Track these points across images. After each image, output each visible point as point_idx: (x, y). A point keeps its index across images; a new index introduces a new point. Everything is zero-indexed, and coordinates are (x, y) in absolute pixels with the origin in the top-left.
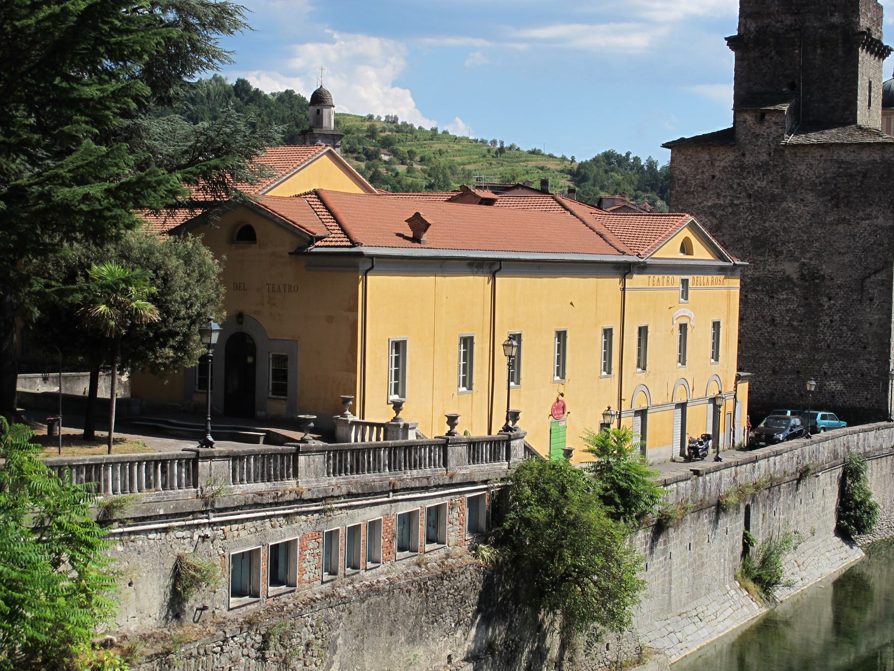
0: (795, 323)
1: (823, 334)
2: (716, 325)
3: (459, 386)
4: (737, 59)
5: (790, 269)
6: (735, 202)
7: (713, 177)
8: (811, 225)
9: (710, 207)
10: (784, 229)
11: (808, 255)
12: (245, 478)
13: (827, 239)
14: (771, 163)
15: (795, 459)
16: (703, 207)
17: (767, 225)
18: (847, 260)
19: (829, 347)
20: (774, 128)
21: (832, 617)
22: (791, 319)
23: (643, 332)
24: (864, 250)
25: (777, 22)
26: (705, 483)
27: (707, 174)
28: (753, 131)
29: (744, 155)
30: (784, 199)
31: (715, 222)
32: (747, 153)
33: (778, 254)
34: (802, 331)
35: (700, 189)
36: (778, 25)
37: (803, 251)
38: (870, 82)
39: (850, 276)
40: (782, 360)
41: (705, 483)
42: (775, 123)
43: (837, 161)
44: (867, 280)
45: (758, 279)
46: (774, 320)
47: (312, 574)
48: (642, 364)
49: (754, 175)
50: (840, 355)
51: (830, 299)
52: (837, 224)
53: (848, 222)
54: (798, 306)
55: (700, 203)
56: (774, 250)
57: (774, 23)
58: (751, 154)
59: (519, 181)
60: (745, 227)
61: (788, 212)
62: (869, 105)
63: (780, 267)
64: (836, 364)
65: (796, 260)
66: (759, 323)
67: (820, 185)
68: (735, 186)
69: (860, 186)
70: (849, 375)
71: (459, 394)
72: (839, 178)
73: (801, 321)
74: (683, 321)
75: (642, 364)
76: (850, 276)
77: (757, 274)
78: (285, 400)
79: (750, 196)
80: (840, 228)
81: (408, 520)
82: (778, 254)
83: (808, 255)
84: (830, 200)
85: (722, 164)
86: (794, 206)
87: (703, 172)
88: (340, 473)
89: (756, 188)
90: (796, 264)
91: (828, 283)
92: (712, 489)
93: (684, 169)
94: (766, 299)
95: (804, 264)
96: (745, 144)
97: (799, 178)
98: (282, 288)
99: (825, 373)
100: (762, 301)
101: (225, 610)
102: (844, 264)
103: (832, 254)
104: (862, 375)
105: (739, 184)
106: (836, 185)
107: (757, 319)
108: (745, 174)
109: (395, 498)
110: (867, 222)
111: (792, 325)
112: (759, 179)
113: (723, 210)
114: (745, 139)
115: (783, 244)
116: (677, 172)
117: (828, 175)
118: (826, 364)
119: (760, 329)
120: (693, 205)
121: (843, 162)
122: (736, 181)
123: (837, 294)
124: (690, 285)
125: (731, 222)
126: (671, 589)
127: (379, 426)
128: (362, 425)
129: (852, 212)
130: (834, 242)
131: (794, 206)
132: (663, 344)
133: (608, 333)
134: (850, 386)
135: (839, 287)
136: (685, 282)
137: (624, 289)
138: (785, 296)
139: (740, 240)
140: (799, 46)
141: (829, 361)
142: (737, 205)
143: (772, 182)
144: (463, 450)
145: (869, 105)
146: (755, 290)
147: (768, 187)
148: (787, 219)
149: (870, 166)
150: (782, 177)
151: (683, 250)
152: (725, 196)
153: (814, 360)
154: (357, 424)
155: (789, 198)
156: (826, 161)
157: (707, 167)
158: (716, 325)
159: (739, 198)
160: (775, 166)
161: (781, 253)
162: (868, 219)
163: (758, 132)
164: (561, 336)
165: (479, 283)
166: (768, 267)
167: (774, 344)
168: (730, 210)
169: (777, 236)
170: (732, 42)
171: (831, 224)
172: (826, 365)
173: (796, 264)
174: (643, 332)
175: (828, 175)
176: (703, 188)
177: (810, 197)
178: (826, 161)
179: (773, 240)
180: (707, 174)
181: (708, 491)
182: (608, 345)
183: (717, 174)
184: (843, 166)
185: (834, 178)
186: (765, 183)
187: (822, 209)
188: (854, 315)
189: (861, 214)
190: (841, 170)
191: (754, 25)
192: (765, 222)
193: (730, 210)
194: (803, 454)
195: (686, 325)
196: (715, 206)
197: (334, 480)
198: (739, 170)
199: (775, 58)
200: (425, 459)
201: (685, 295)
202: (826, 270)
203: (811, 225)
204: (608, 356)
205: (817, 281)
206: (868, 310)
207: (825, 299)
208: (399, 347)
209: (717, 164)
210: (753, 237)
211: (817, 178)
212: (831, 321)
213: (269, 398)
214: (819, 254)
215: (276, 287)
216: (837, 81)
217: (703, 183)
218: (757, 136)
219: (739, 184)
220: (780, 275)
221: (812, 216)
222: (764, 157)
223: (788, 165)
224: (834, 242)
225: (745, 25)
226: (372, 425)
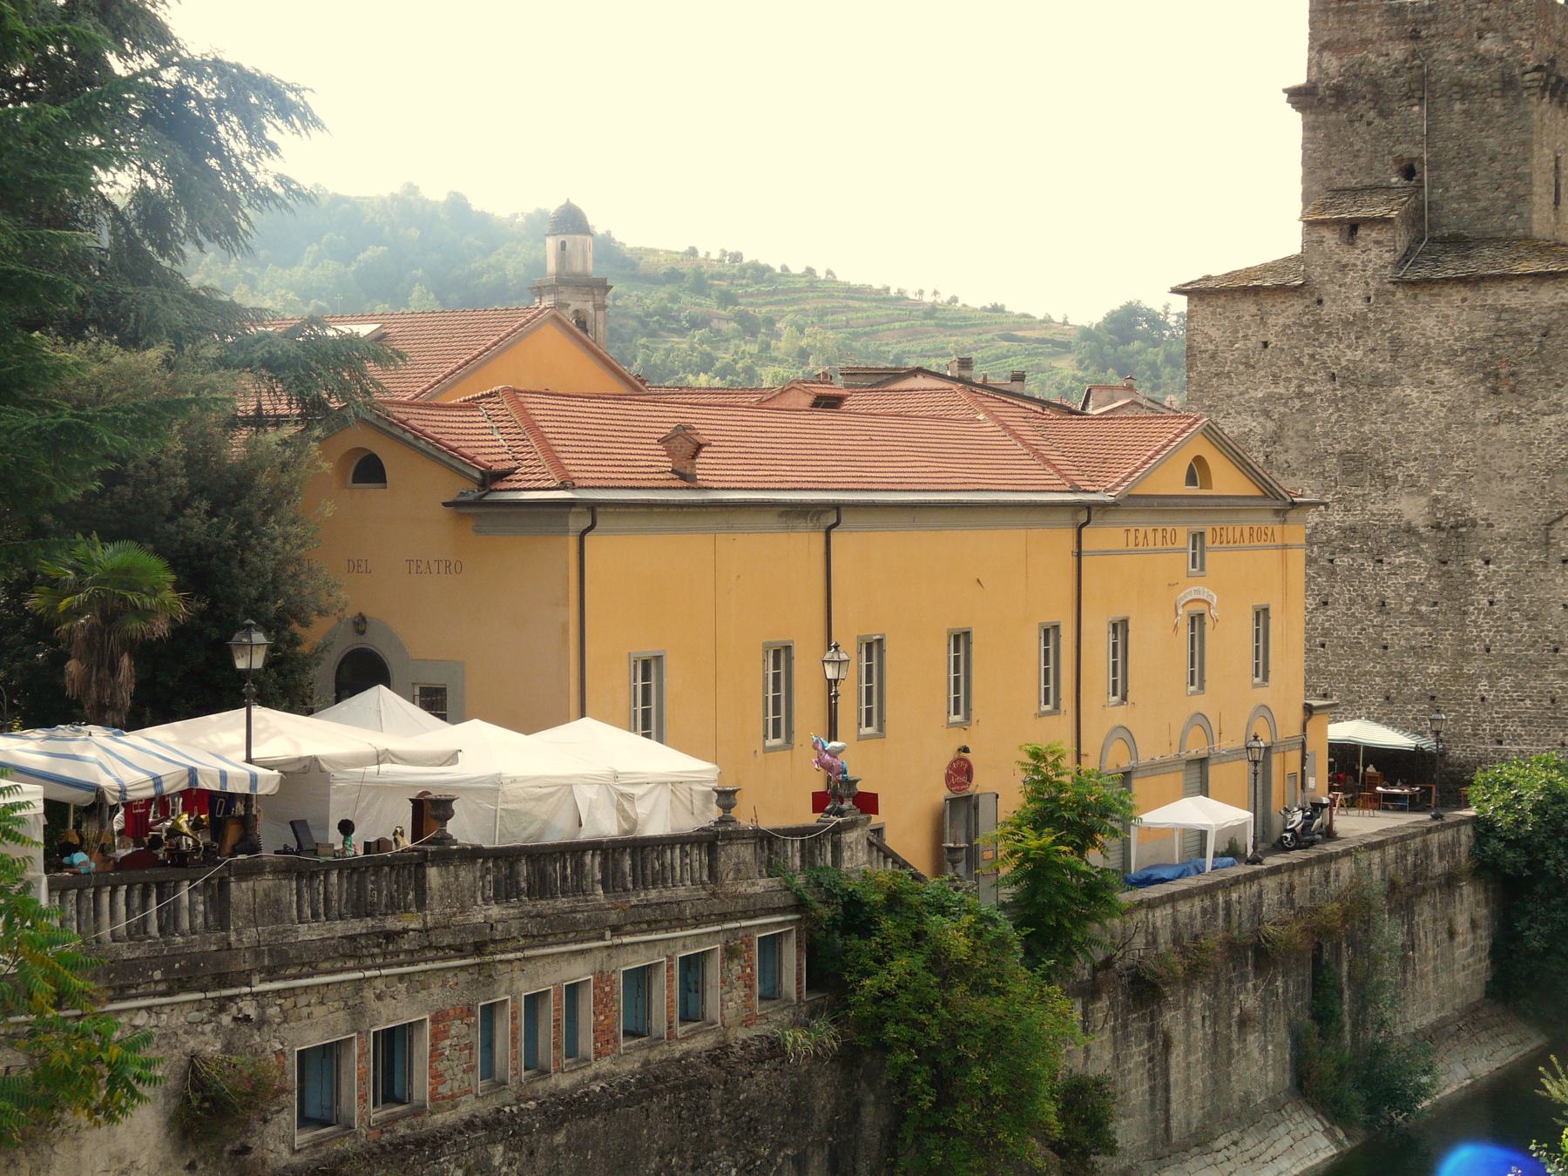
0: (1423, 608)
1: (1476, 627)
2: (1262, 614)
3: (766, 737)
4: (1306, 127)
5: (1412, 509)
6: (1307, 389)
7: (1266, 345)
8: (1448, 427)
9: (1261, 401)
10: (1399, 438)
11: (1445, 483)
12: (321, 910)
13: (1479, 452)
14: (1370, 315)
15: (1410, 859)
16: (1248, 401)
17: (1366, 428)
18: (1516, 490)
19: (1488, 650)
20: (1375, 251)
21: (653, 982)
22: (1416, 602)
23: (1120, 628)
24: (1550, 471)
25: (1380, 55)
26: (1228, 904)
27: (1254, 339)
28: (1336, 258)
29: (1320, 302)
30: (1396, 381)
31: (1271, 426)
32: (1325, 298)
33: (1387, 482)
34: (1436, 622)
35: (1241, 367)
37: (1435, 476)
38: (1557, 159)
39: (1525, 519)
40: (1402, 676)
41: (1228, 904)
42: (1377, 242)
43: (1493, 308)
44: (1557, 526)
45: (1353, 529)
46: (1383, 604)
47: (456, 1084)
48: (1120, 688)
49: (1340, 340)
50: (1510, 666)
51: (1487, 563)
52: (1496, 424)
53: (1518, 420)
54: (1429, 576)
55: (1241, 394)
56: (1382, 476)
57: (1372, 57)
58: (1334, 301)
59: (912, 363)
60: (1326, 434)
61: (1404, 405)
62: (1557, 202)
63: (1392, 507)
64: (1502, 682)
65: (1423, 491)
66: (1357, 610)
67: (1464, 351)
68: (1306, 360)
69: (1539, 352)
70: (1528, 702)
71: (767, 750)
73: (1435, 604)
74: (1197, 608)
75: (1120, 688)
76: (1525, 519)
77: (1350, 520)
79: (1333, 377)
80: (1503, 431)
81: (640, 979)
82: (1387, 482)
83: (1445, 483)
84: (1482, 381)
85: (1281, 321)
86: (1415, 394)
87: (1245, 337)
88: (508, 898)
89: (1344, 363)
90: (1423, 501)
91: (1485, 533)
92: (1245, 916)
93: (1213, 332)
94: (1369, 567)
95: (1436, 500)
96: (1323, 283)
97: (1422, 342)
98: (434, 567)
99: (1483, 699)
100: (1361, 568)
101: (286, 1154)
103: (1488, 480)
104: (1553, 701)
105: (1312, 356)
107: (1352, 602)
108: (1323, 338)
109: (617, 941)
110: (1553, 418)
111: (1419, 612)
112: (1349, 347)
113: (1285, 405)
115: (1397, 464)
116: (1198, 338)
117: (1477, 335)
119: (1360, 621)
120: (1230, 397)
122: (1308, 351)
124: (1208, 542)
125: (1301, 426)
126: (1168, 1101)
129: (1523, 401)
130: (1492, 457)
131: (1415, 394)
132: (1157, 650)
133: (1050, 633)
134: (1530, 723)
136: (1198, 537)
137: (1079, 555)
138: (1403, 559)
139: (1318, 459)
140: (1421, 99)
141: (1489, 677)
142: (1310, 395)
143: (1373, 350)
144: (746, 852)
145: (1557, 202)
146: (1347, 550)
147: (1366, 361)
148: (1403, 418)
149: (1555, 315)
150: (1392, 340)
151: (1191, 479)
152: (1288, 380)
153: (1462, 675)
155: (1406, 380)
157: (1254, 328)
158: (1262, 614)
159: (1312, 382)
160: (1379, 321)
161: (1394, 479)
162: (1554, 412)
163: (1344, 261)
164: (961, 640)
165: (805, 543)
166: (1370, 507)
167: (1386, 648)
168: (1298, 404)
169: (1385, 450)
170: (1300, 97)
171: (1486, 424)
172: (1483, 685)
173: (1423, 501)
174: (1120, 628)
175: (1477, 335)
176: (1247, 365)
177: (1445, 375)
178: (1473, 308)
179: (1380, 456)
180: (1254, 339)
181: (1235, 919)
182: (1051, 656)
183: (1272, 339)
184: (1504, 316)
185: (1489, 340)
186: (1359, 353)
188: (1532, 590)
189: (1540, 404)
190: (1501, 324)
191: (1335, 63)
192: (1362, 425)
193: (1298, 404)
194: (1425, 846)
195: (1201, 615)
196: (1269, 397)
197: (495, 911)
198: (1311, 331)
199: (1376, 122)
200: (673, 868)
201: (1198, 561)
202: (1479, 509)
203: (1448, 427)
204: (1051, 676)
206: (1559, 580)
207: (1480, 562)
209: (1271, 321)
210: (1341, 454)
211: (1456, 340)
212: (1491, 603)
214: (1462, 479)
215: (423, 566)
216: (1492, 159)
217: (1247, 357)
218: (1343, 268)
219: (1312, 356)
220: (1393, 521)
221: (1450, 410)
222: (1359, 306)
223: (1401, 318)
224: (1492, 457)
225: (1319, 65)
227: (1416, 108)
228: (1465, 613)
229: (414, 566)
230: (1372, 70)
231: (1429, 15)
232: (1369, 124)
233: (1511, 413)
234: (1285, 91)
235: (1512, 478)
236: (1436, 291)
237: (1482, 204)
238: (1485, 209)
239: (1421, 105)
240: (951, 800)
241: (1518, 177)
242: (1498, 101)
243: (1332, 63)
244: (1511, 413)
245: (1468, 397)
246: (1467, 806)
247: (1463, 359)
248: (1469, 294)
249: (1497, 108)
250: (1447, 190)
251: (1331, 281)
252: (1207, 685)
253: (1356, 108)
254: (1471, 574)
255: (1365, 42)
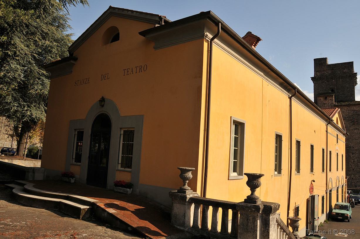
2: (342, 155)
18: (358, 141)
19: (353, 170)
20: (330, 101)
28: (323, 102)
36: (327, 73)
43: (353, 110)
51: (353, 154)
57: (325, 73)
64: (356, 175)
67: (347, 118)
72: (353, 115)
78: (80, 165)
84: (351, 123)
99: (352, 178)
102: (357, 143)
106: (353, 118)
114: (321, 105)
118: (353, 175)
121: (355, 111)
123: (355, 152)
127: (226, 206)
128: (203, 203)
135: (356, 150)
141: (353, 174)
154: (197, 201)
156: (349, 110)
158: (342, 155)
164: (312, 147)
171: (352, 130)
178: (349, 110)
184: (355, 112)
185: (352, 116)
187: (349, 125)
190: (354, 113)
191: (319, 74)
205: (348, 148)
208: (239, 127)
211: (346, 116)
212: (354, 161)
213: (118, 170)
215: (130, 71)
216: (347, 88)
224: (354, 136)
225: (316, 74)
226: (216, 204)
227: (333, 80)
228: (349, 163)
229: (126, 71)
230: (325, 75)
231: (335, 66)
232: (325, 83)
233: (357, 128)
234: (311, 78)
235: (358, 139)
236: (342, 107)
237: (346, 95)
238: (346, 96)
239: (334, 80)
240: (311, 196)
241: (352, 91)
242: (348, 79)
243: (318, 74)
244: (357, 128)
245: (349, 125)
246: (26, 157)
247: (347, 119)
248: (348, 108)
249: (348, 80)
250: (339, 93)
251: (322, 106)
252: (301, 171)
253: (323, 81)
254: (350, 156)
255: (324, 70)
